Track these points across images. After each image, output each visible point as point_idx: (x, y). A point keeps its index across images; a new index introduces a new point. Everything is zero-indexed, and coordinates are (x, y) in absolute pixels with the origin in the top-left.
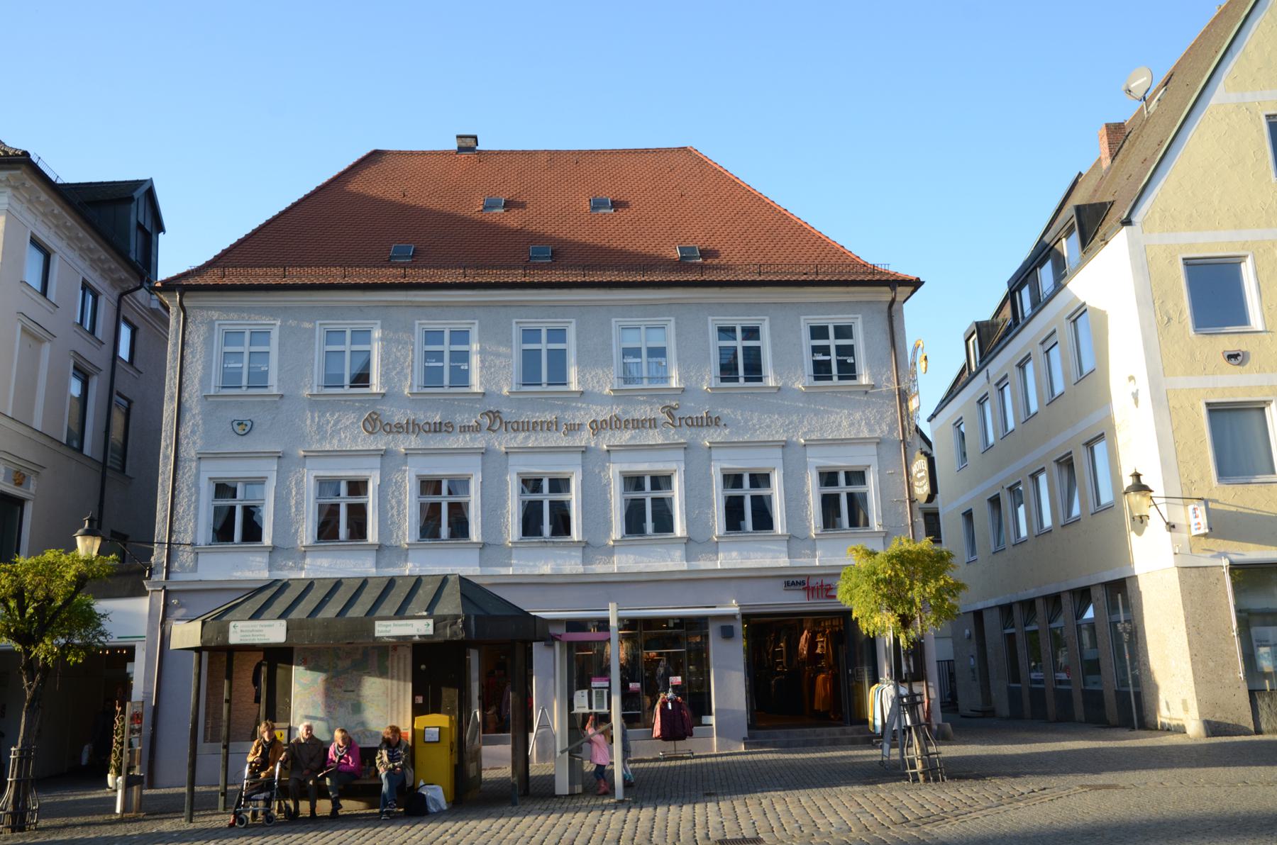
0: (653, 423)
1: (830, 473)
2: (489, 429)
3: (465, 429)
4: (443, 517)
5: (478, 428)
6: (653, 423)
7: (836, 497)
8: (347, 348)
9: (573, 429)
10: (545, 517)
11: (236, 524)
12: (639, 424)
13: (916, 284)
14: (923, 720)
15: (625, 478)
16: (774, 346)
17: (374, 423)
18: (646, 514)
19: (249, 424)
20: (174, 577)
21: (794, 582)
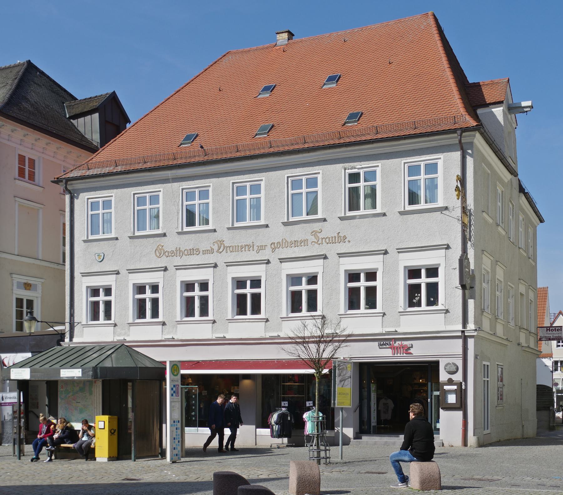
0: (304, 242)
1: (94, 290)
2: (218, 251)
3: (205, 252)
4: (302, 300)
5: (211, 251)
6: (304, 242)
7: (299, 293)
8: (304, 190)
9: (262, 248)
10: (146, 307)
11: (99, 311)
12: (296, 244)
13: (53, 182)
14: (366, 420)
15: (409, 271)
16: (383, 184)
17: (160, 252)
18: (195, 304)
19: (103, 255)
20: (75, 340)
21: (384, 341)
